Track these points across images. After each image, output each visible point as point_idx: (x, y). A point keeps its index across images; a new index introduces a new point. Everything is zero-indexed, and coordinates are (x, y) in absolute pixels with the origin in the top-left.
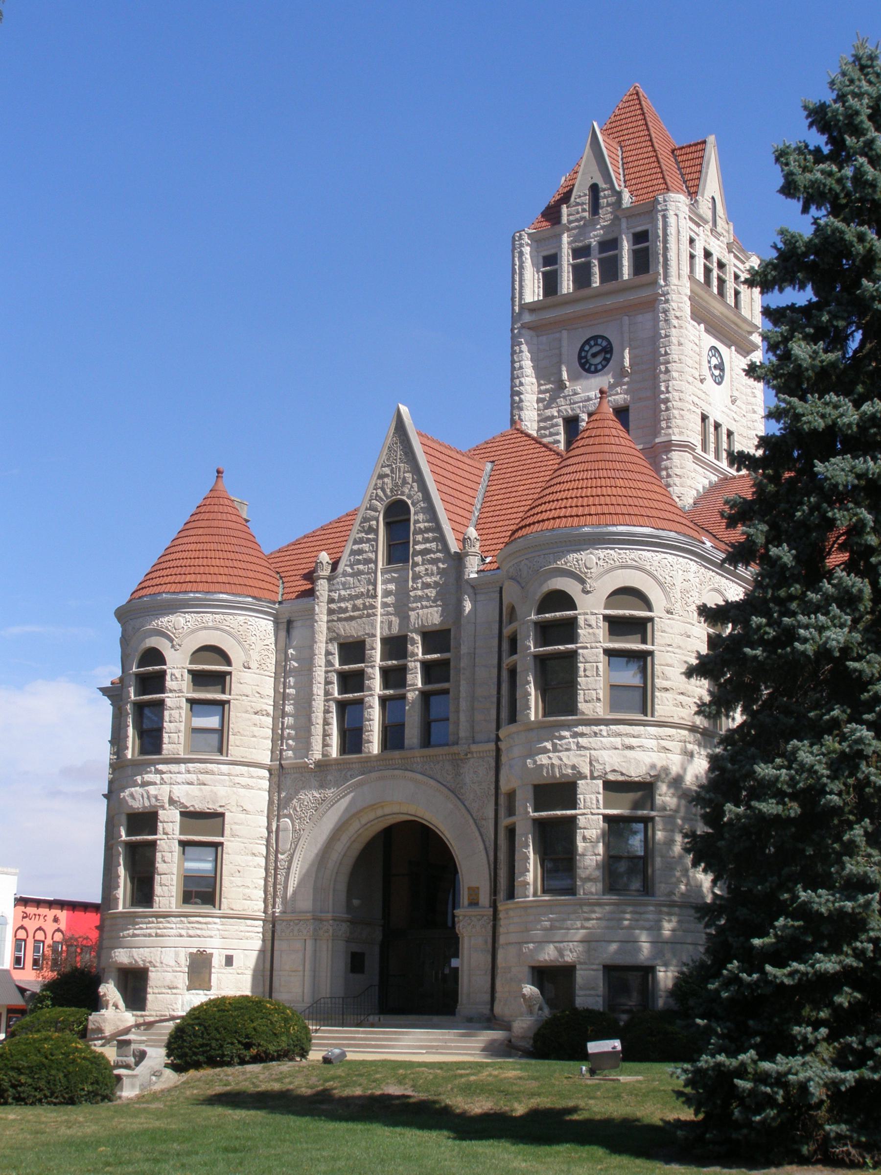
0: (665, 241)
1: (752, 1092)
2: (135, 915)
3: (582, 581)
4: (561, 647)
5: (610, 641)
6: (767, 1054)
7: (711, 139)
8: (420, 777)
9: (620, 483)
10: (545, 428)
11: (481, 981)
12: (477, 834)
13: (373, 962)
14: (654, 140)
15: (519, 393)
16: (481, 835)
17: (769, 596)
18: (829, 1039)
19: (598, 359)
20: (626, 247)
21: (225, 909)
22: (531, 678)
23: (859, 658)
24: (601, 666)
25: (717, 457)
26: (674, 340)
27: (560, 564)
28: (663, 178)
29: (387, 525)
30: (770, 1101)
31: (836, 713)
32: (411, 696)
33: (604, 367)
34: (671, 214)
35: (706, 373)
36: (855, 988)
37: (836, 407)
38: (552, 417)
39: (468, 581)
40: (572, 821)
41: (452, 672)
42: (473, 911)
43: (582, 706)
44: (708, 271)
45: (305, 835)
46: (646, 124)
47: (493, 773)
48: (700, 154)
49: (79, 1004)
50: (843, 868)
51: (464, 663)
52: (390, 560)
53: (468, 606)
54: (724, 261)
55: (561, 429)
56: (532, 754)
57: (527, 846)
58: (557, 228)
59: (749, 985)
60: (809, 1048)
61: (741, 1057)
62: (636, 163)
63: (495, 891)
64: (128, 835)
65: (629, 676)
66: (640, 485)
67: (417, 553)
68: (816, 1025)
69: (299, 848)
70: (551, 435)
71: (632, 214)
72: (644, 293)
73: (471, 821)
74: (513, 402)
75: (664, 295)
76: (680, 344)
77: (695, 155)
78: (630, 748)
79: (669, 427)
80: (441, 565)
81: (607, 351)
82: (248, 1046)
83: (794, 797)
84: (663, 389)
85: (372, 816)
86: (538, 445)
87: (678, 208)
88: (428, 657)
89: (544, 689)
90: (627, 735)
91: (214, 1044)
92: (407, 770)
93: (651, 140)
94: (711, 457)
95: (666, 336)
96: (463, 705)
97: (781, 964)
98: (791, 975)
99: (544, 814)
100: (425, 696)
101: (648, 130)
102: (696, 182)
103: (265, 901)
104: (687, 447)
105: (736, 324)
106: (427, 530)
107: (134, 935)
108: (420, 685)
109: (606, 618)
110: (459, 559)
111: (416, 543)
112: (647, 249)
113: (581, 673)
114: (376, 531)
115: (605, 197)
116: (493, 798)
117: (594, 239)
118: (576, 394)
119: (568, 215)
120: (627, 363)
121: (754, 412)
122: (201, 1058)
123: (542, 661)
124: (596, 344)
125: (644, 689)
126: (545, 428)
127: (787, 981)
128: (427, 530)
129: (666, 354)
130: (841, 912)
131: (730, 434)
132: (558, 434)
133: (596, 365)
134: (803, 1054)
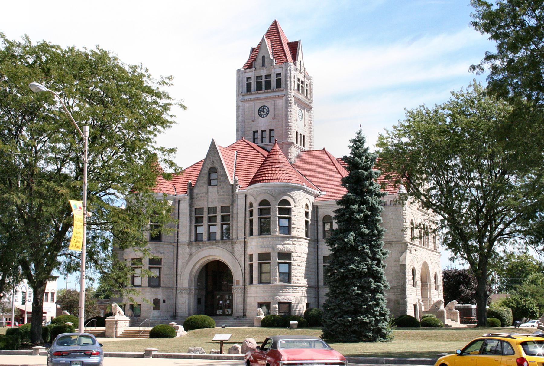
11: (241, 306)
17: (371, 303)
25: (300, 145)
27: (290, 194)
33: (266, 116)
41: (231, 219)
44: (299, 85)
47: (243, 248)
51: (235, 216)
63: (244, 281)
87: (291, 68)
131: (304, 136)
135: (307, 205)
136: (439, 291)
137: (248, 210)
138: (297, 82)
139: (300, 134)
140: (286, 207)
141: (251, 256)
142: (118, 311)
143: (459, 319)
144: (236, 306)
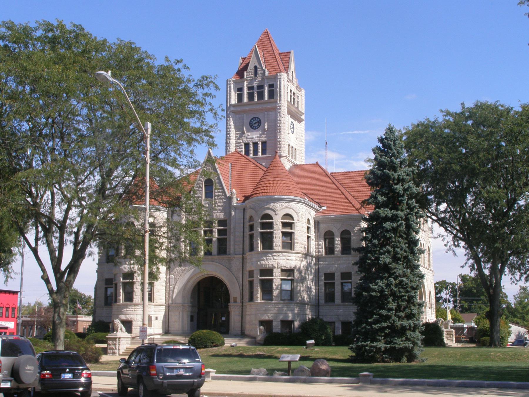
0: (280, 89)
1: (369, 349)
2: (127, 305)
3: (275, 212)
4: (269, 230)
5: (282, 229)
6: (372, 342)
7: (292, 52)
8: (217, 264)
9: (284, 182)
10: (238, 146)
12: (236, 281)
13: (195, 319)
14: (275, 51)
15: (229, 134)
16: (238, 282)
18: (384, 339)
19: (256, 125)
20: (266, 89)
21: (155, 303)
22: (259, 239)
23: (391, 264)
24: (280, 236)
26: (282, 122)
27: (268, 206)
28: (279, 66)
29: (205, 186)
30: (372, 351)
31: (386, 275)
32: (214, 239)
33: (258, 128)
34: (282, 80)
35: (290, 131)
36: (389, 329)
37: (387, 211)
38: (240, 143)
39: (233, 206)
40: (272, 280)
42: (235, 304)
43: (275, 247)
44: (291, 96)
45: (179, 280)
46: (271, 45)
48: (289, 56)
49: (222, 333)
50: (388, 306)
51: (232, 230)
52: (206, 197)
53: (233, 213)
54: (295, 92)
55: (243, 147)
56: (260, 261)
57: (258, 287)
58: (242, 80)
59: (368, 329)
60: (380, 341)
61: (367, 343)
62: (269, 59)
63: (242, 298)
64: (123, 280)
65: (287, 240)
66: (290, 183)
67: (215, 196)
68: (382, 336)
69: (177, 284)
70: (240, 148)
71: (268, 78)
72: (272, 106)
73: (234, 278)
74: (227, 137)
75: (279, 107)
76: (284, 123)
77: (287, 56)
78: (288, 260)
79: (280, 150)
80: (224, 200)
81: (259, 122)
82: (213, 343)
83: (378, 292)
84: (278, 137)
85: (201, 275)
86: (250, 162)
87: (284, 78)
88: (220, 228)
89: (263, 242)
90: (287, 256)
91: (204, 343)
92: (213, 261)
93: (273, 51)
94: (290, 158)
95: (280, 120)
96: (232, 243)
97: (375, 325)
98: (377, 327)
99: (263, 278)
100: (219, 240)
101: (272, 47)
102: (287, 66)
103: (166, 300)
104: (285, 157)
105: (297, 113)
106: (219, 189)
107: (127, 311)
108: (217, 236)
109: (282, 222)
110: (230, 199)
111: (215, 192)
112: (273, 90)
113: (275, 238)
114: (202, 188)
115: (259, 71)
116: (242, 271)
117: (255, 84)
118: (248, 136)
119: (247, 75)
120: (266, 127)
121: (302, 142)
122: (201, 346)
123: (262, 234)
124: (255, 120)
125: (291, 243)
126: (238, 146)
127: (377, 328)
128: (219, 189)
129: (280, 126)
130: (388, 315)
131: (295, 149)
132: (242, 148)
133: (255, 127)
134: (379, 342)
135: (308, 220)
136: (433, 310)
137: (247, 224)
138: (289, 94)
139: (292, 147)
140: (268, 221)
141: (251, 273)
142: (119, 328)
143: (454, 339)
144: (233, 324)
